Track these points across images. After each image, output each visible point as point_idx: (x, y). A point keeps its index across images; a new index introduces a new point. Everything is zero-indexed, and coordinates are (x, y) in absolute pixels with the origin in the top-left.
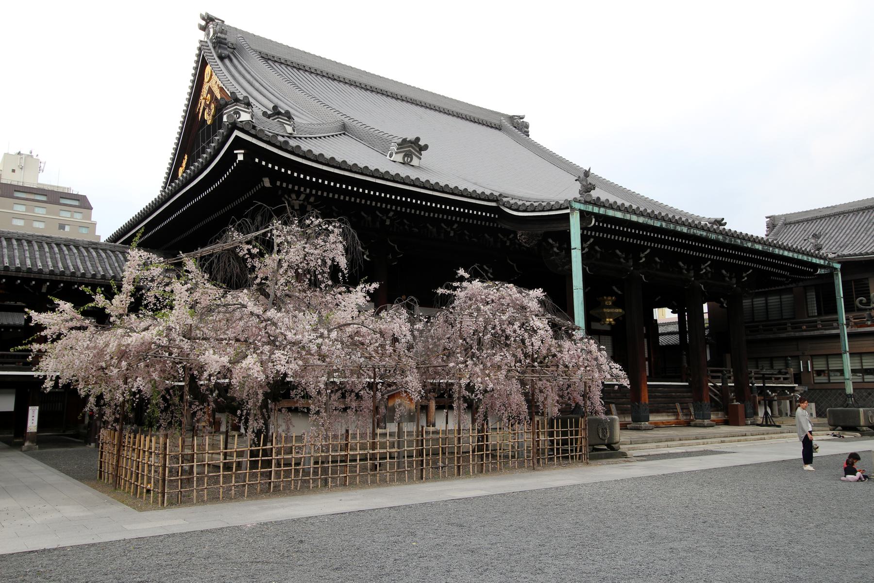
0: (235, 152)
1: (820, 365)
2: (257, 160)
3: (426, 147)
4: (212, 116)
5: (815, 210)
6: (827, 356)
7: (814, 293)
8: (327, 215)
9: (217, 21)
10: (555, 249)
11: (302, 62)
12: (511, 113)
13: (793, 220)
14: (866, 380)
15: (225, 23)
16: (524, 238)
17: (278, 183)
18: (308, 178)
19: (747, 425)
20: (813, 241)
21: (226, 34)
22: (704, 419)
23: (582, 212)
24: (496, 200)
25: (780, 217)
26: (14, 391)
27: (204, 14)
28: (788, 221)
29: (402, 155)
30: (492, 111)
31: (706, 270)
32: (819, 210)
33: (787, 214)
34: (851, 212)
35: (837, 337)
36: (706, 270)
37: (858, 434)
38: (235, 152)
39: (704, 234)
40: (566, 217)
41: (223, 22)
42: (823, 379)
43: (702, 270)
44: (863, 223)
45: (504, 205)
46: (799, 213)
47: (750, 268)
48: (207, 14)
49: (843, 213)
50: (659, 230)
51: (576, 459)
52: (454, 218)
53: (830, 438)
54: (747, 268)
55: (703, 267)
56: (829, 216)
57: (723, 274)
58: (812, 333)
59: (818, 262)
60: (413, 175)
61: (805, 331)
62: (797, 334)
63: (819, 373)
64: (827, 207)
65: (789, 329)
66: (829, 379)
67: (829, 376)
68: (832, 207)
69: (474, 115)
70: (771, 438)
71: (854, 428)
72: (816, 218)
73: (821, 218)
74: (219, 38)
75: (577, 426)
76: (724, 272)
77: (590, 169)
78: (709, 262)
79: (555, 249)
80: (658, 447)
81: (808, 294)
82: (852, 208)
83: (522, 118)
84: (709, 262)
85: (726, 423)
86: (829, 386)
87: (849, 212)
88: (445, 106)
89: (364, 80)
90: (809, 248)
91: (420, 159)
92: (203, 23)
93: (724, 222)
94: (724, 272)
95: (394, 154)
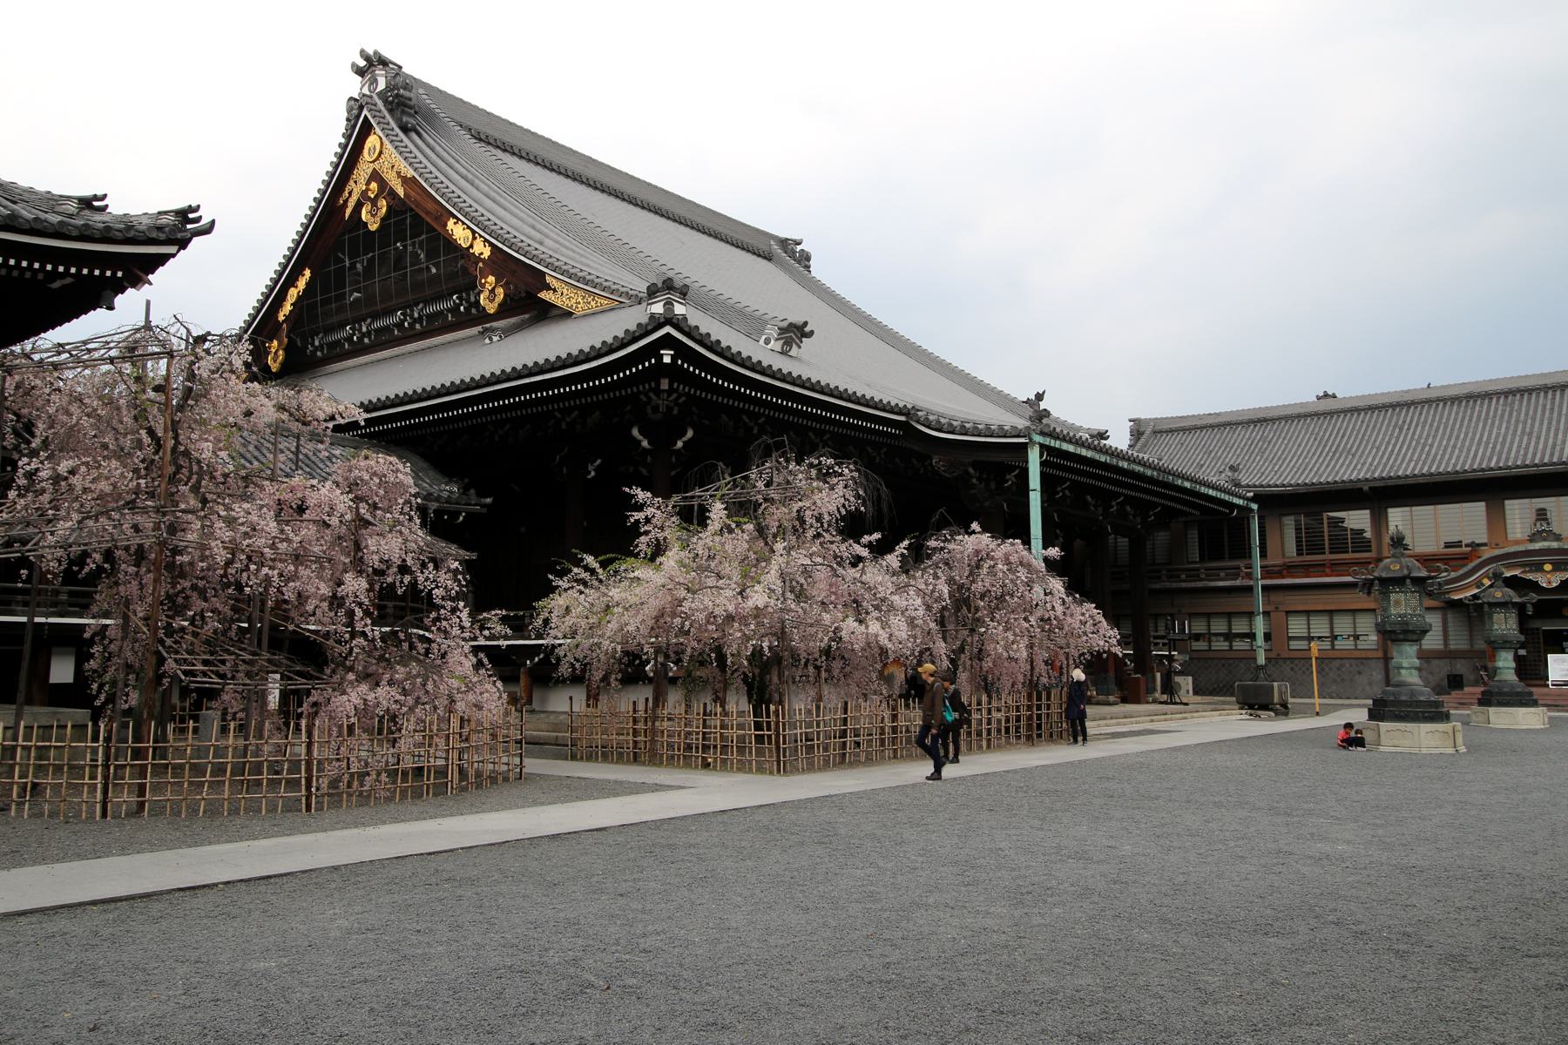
0: (662, 352)
1: (1199, 627)
2: (680, 362)
3: (812, 333)
4: (381, 219)
5: (1193, 416)
6: (1229, 616)
7: (1196, 532)
8: (841, 455)
9: (391, 66)
10: (974, 481)
11: (508, 139)
12: (783, 234)
13: (1165, 427)
14: (1359, 647)
15: (403, 70)
16: (943, 466)
17: (675, 385)
18: (703, 375)
19: (1148, 703)
20: (1230, 474)
21: (410, 91)
22: (1108, 694)
23: (1042, 446)
24: (907, 414)
25: (1148, 421)
26: (73, 650)
27: (371, 53)
28: (1158, 428)
29: (781, 342)
30: (758, 230)
31: (1064, 494)
32: (1199, 417)
33: (1156, 419)
34: (1239, 424)
35: (1250, 589)
36: (1064, 494)
37: (1273, 714)
38: (662, 352)
39: (1142, 469)
40: (1023, 448)
41: (400, 67)
42: (1200, 645)
43: (1007, 481)
44: (1256, 442)
45: (918, 422)
46: (1172, 418)
47: (1122, 494)
48: (376, 53)
49: (1229, 424)
50: (1151, 480)
51: (428, 793)
52: (762, 410)
53: (1243, 718)
54: (1156, 505)
55: (1008, 477)
56: (1212, 426)
57: (1087, 501)
58: (1193, 585)
59: (1052, 445)
60: (796, 369)
61: (1184, 581)
62: (1174, 585)
63: (1197, 637)
64: (1210, 414)
65: (1164, 578)
66: (1210, 646)
67: (1210, 641)
68: (1215, 414)
69: (710, 225)
70: (1192, 717)
71: (1265, 707)
72: (1196, 428)
73: (1202, 428)
74: (402, 96)
75: (1048, 698)
76: (1089, 498)
77: (1044, 392)
78: (1068, 483)
79: (974, 481)
80: (1099, 726)
81: (1189, 532)
82: (1240, 418)
83: (799, 244)
84: (1068, 483)
85: (1125, 700)
86: (1211, 655)
87: (1237, 424)
88: (497, 135)
89: (591, 173)
90: (1221, 480)
91: (800, 347)
92: (362, 63)
93: (807, 329)
94: (1089, 498)
95: (772, 342)
